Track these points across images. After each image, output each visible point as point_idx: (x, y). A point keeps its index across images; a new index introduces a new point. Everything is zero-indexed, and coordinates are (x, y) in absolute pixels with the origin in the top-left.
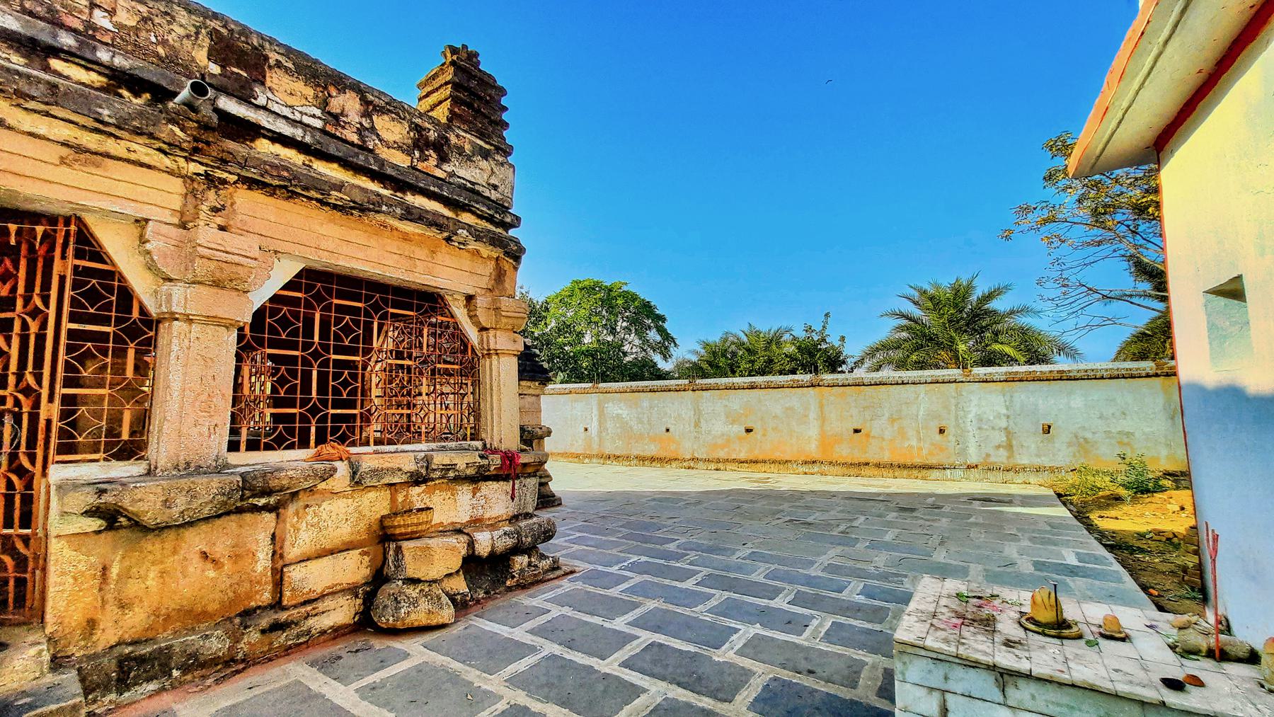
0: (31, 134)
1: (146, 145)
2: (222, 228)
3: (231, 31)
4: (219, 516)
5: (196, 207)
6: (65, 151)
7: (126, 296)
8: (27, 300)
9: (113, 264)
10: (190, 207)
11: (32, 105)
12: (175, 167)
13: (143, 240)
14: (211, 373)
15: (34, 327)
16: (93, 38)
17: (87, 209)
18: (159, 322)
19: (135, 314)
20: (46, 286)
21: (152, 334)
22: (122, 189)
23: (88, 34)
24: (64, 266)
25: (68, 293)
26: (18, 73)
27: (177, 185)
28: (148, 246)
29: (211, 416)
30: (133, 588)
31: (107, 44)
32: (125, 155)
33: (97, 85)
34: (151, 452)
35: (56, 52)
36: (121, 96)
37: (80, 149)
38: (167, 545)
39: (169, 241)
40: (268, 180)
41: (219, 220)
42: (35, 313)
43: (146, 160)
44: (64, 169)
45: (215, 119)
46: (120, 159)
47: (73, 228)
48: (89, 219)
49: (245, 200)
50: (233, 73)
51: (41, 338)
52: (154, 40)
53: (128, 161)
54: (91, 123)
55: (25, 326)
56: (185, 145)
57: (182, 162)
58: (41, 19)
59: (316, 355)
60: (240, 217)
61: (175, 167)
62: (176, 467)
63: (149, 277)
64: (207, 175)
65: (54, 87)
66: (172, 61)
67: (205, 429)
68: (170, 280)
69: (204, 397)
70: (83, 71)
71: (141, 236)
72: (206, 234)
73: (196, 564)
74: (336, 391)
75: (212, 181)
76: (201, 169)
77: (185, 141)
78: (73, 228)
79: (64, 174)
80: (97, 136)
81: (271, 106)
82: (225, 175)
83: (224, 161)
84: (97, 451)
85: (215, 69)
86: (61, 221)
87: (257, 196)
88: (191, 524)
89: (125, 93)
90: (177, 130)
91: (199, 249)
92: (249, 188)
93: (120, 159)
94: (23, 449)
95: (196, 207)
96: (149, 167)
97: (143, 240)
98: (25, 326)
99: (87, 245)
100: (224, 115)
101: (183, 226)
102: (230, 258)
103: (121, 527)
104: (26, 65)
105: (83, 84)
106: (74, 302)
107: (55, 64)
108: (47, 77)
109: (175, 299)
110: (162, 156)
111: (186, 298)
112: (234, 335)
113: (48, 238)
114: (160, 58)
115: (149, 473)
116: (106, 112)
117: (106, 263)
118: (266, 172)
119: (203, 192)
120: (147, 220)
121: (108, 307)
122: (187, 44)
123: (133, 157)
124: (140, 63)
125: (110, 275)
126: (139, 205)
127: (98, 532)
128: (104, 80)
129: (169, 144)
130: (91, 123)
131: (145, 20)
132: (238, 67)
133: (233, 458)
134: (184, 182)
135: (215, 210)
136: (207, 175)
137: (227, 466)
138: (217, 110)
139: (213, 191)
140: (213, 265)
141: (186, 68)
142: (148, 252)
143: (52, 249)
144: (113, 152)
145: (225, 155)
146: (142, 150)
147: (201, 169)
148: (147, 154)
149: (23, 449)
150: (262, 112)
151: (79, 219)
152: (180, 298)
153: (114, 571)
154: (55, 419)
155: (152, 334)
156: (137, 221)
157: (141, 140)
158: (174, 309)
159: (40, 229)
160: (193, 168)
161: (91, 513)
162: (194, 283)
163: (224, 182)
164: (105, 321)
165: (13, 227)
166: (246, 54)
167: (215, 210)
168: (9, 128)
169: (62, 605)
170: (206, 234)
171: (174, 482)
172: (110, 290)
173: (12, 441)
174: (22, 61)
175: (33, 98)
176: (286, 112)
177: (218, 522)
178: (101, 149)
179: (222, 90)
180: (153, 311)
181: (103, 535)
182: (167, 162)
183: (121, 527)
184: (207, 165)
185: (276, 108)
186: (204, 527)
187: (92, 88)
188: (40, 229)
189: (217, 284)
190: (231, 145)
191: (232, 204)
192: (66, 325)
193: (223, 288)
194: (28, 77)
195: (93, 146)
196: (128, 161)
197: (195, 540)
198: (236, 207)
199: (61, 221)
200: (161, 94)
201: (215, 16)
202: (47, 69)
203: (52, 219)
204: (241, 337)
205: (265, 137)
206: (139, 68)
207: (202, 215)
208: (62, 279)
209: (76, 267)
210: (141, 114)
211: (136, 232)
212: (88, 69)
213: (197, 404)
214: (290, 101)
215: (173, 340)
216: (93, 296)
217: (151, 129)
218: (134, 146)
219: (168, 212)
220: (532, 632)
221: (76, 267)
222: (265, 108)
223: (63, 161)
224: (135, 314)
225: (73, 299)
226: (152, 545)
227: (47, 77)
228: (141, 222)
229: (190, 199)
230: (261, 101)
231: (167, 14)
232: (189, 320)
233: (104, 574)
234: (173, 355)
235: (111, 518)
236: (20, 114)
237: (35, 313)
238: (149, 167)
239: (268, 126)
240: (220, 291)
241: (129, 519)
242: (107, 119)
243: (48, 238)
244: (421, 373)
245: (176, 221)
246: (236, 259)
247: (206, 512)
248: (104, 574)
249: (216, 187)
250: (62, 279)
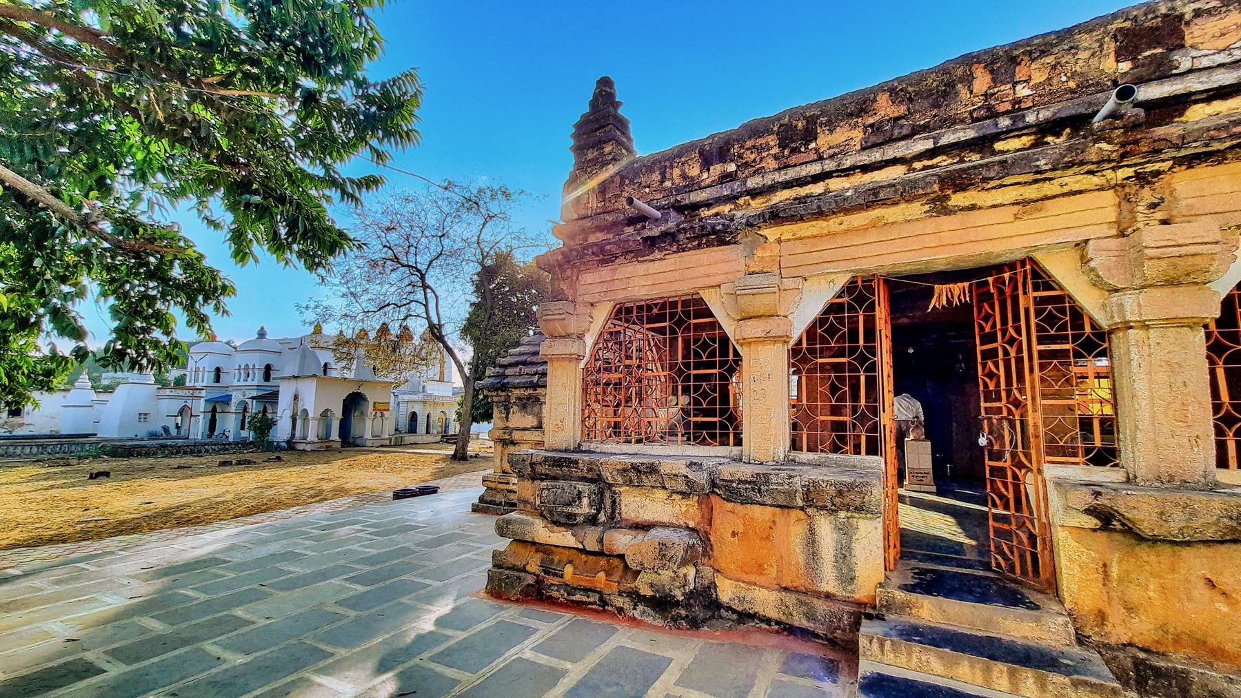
0: (994, 206)
1: (1075, 174)
2: (1164, 222)
3: (1135, 19)
4: (1222, 542)
5: (1131, 212)
6: (1017, 208)
7: (1077, 314)
8: (1004, 332)
9: (1062, 289)
10: (1125, 213)
11: (992, 184)
12: (1104, 182)
13: (1085, 260)
14: (1180, 379)
15: (1013, 354)
16: (1020, 109)
17: (1037, 248)
18: (1110, 332)
19: (1088, 329)
20: (1016, 318)
21: (1106, 345)
22: (1061, 222)
23: (1017, 109)
24: (1027, 301)
25: (1033, 321)
26: (982, 166)
27: (1109, 197)
28: (1092, 264)
29: (1188, 427)
30: (1135, 595)
31: (1030, 108)
32: (1059, 191)
33: (1028, 144)
34: (1125, 457)
35: (997, 137)
36: (1047, 143)
37: (1025, 202)
38: (1162, 559)
39: (1110, 253)
40: (1216, 146)
41: (1160, 215)
42: (1011, 341)
43: (1076, 187)
44: (1018, 222)
45: (1141, 112)
46: (1054, 197)
47: (1028, 267)
48: (1038, 256)
49: (1187, 184)
50: (1146, 58)
51: (1019, 361)
52: (1064, 79)
53: (1063, 195)
54: (1031, 177)
55: (1006, 353)
56: (1114, 156)
57: (1109, 174)
58: (985, 119)
59: (680, 323)
60: (1184, 203)
61: (1104, 182)
62: (1159, 478)
63: (1095, 293)
64: (1137, 174)
65: (1003, 163)
66: (1088, 86)
67: (1186, 441)
68: (1117, 290)
69: (1177, 406)
70: (1016, 140)
71: (1082, 257)
72: (1152, 234)
73: (1200, 591)
74: (697, 355)
75: (1144, 178)
76: (1130, 172)
77: (1113, 152)
78: (1028, 267)
79: (1019, 227)
80: (1036, 186)
81: (1197, 65)
82: (1156, 166)
83: (1158, 151)
84: (1075, 455)
85: (1125, 66)
86: (1019, 266)
87: (1203, 171)
88: (1188, 544)
89: (1049, 139)
90: (1104, 146)
91: (1146, 251)
92: (1190, 167)
93: (1054, 197)
94: (1020, 449)
95: (1131, 212)
96: (1081, 192)
97: (1085, 260)
98: (1006, 353)
99: (1041, 279)
100: (1148, 105)
101: (1122, 234)
102: (1183, 250)
103: (1115, 530)
104: (981, 158)
105: (1018, 150)
106: (1040, 328)
107: (998, 146)
108: (997, 158)
109: (1128, 307)
110: (1090, 176)
111: (1139, 305)
112: (1202, 332)
113: (1013, 280)
114: (1073, 91)
115: (1128, 480)
116: (1043, 162)
117: (1054, 289)
118: (1213, 139)
119: (1136, 193)
120: (1086, 241)
121: (1063, 327)
122: (1094, 62)
123: (1066, 189)
124: (1060, 106)
125: (1060, 299)
126: (1077, 230)
127: (1094, 530)
128: (1033, 137)
129: (1098, 163)
130: (1031, 177)
131: (1054, 67)
132: (1150, 48)
133: (1223, 476)
134: (1116, 191)
135: (1153, 206)
136: (1137, 174)
137: (1217, 484)
138: (1137, 105)
139: (1147, 188)
140: (1164, 264)
141: (1098, 84)
142: (1092, 270)
143: (1015, 289)
144: (1049, 193)
145: (1157, 146)
146: (1073, 180)
147: (1130, 172)
148: (1077, 182)
149: (1020, 449)
150: (1191, 76)
151: (1031, 259)
152: (1132, 306)
153: (1114, 571)
154: (1040, 424)
155: (1106, 345)
156: (1077, 245)
157: (1070, 172)
158: (1129, 318)
159: (1007, 275)
160: (1122, 173)
161: (1090, 511)
162: (1144, 287)
163: (1157, 173)
164: (1064, 339)
165: (990, 279)
166: (1157, 28)
167: (1153, 206)
168: (980, 208)
169: (1074, 587)
170: (1152, 234)
171: (1168, 495)
172: (1063, 311)
173: (1011, 442)
174: (978, 156)
175: (992, 179)
176: (1222, 58)
177: (1223, 548)
178: (1041, 195)
179: (1142, 81)
180: (1104, 324)
181: (1098, 533)
182: (1096, 180)
183: (1115, 530)
184: (1136, 165)
185: (1205, 62)
186: (1203, 550)
187: (1029, 148)
188: (1007, 275)
189: (1172, 282)
190: (1160, 131)
191: (1171, 193)
192: (1036, 348)
193: (1179, 284)
194: (986, 165)
195: (1033, 196)
196: (1063, 195)
197: (1197, 563)
198: (1176, 194)
199: (1019, 266)
200: (1078, 123)
201: (1115, 16)
202: (994, 153)
203: (1012, 266)
204: (1208, 335)
205: (1196, 102)
206: (1059, 110)
207: (1140, 217)
208: (1027, 311)
209: (1035, 298)
210: (1070, 149)
211: (1076, 254)
212: (1019, 136)
213: (1170, 413)
214: (1221, 44)
215: (1133, 350)
216: (1051, 320)
217: (1080, 157)
218: (1066, 180)
219: (1105, 226)
220: (448, 638)
221: (1035, 298)
222: (1190, 71)
223: (1016, 217)
224: (1088, 329)
225: (1037, 325)
226: (1143, 552)
227: (997, 158)
228: (1082, 245)
229: (1125, 205)
230: (1185, 64)
231: (1071, 48)
232: (1145, 326)
233: (1105, 572)
234: (1134, 364)
235: (1106, 519)
236: (984, 194)
237: (1011, 341)
238: (1081, 192)
239: (1201, 87)
240: (1175, 289)
241: (1123, 524)
242: (1044, 168)
243: (1013, 280)
244: (29, 306)
245: (1114, 232)
246: (1192, 249)
247: (1209, 534)
248: (1105, 572)
249: (1149, 183)
250: (1027, 311)
